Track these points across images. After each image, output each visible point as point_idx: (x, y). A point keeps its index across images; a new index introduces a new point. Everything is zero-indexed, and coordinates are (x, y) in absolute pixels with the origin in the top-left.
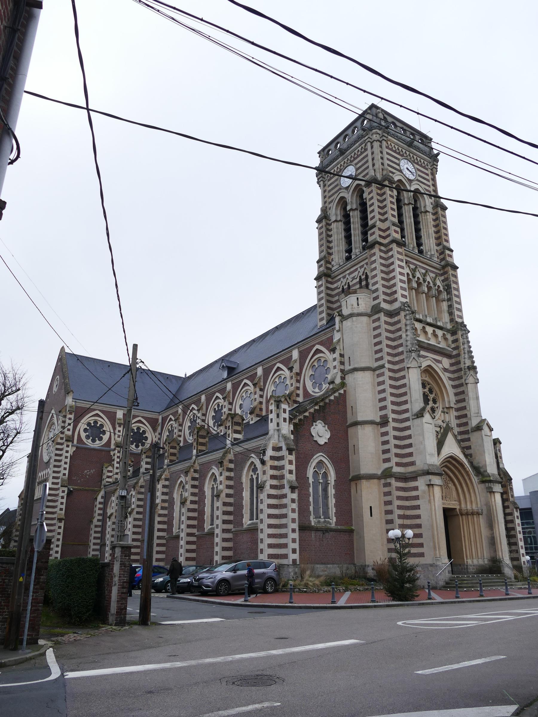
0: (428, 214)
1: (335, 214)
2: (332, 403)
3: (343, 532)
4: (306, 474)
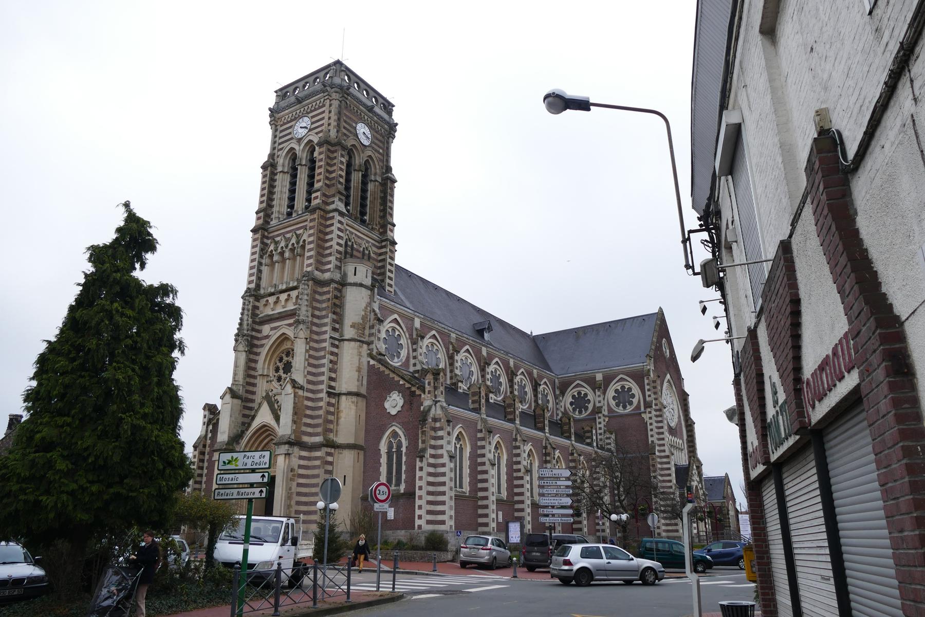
1: (282, 163)
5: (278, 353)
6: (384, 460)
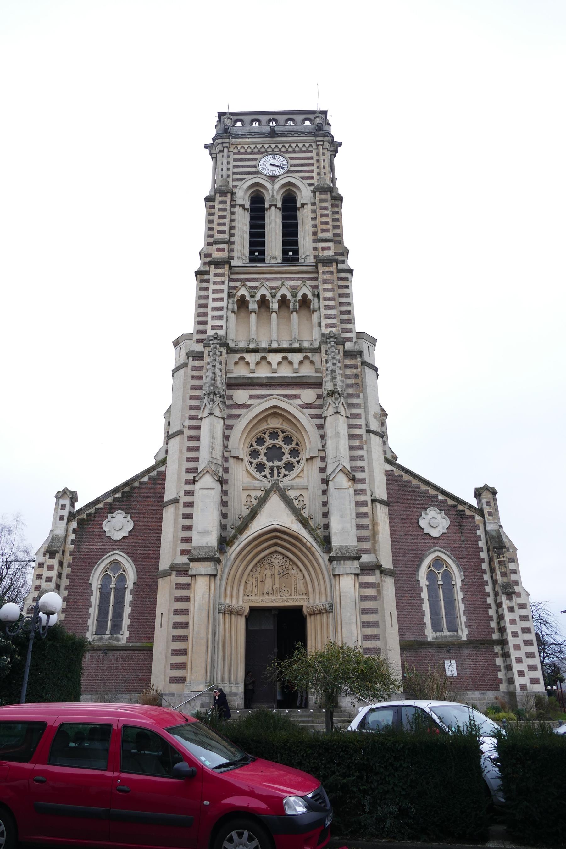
0: (305, 206)
2: (144, 486)
3: (140, 650)
4: (88, 580)
5: (257, 431)
6: (95, 599)
